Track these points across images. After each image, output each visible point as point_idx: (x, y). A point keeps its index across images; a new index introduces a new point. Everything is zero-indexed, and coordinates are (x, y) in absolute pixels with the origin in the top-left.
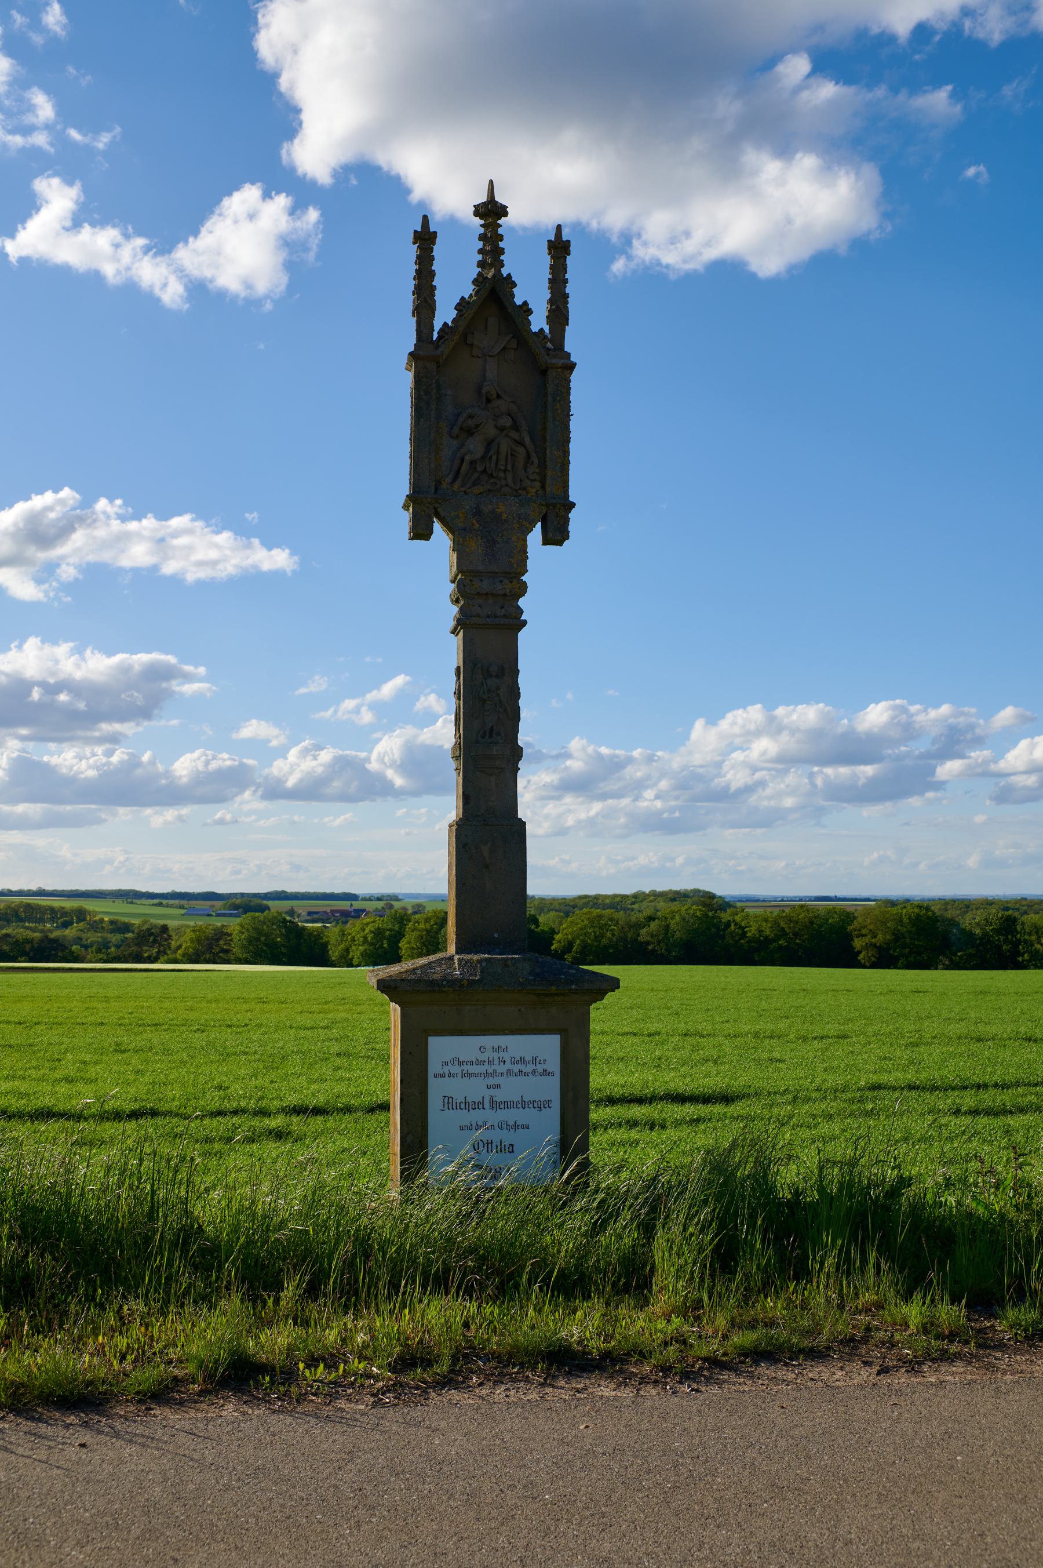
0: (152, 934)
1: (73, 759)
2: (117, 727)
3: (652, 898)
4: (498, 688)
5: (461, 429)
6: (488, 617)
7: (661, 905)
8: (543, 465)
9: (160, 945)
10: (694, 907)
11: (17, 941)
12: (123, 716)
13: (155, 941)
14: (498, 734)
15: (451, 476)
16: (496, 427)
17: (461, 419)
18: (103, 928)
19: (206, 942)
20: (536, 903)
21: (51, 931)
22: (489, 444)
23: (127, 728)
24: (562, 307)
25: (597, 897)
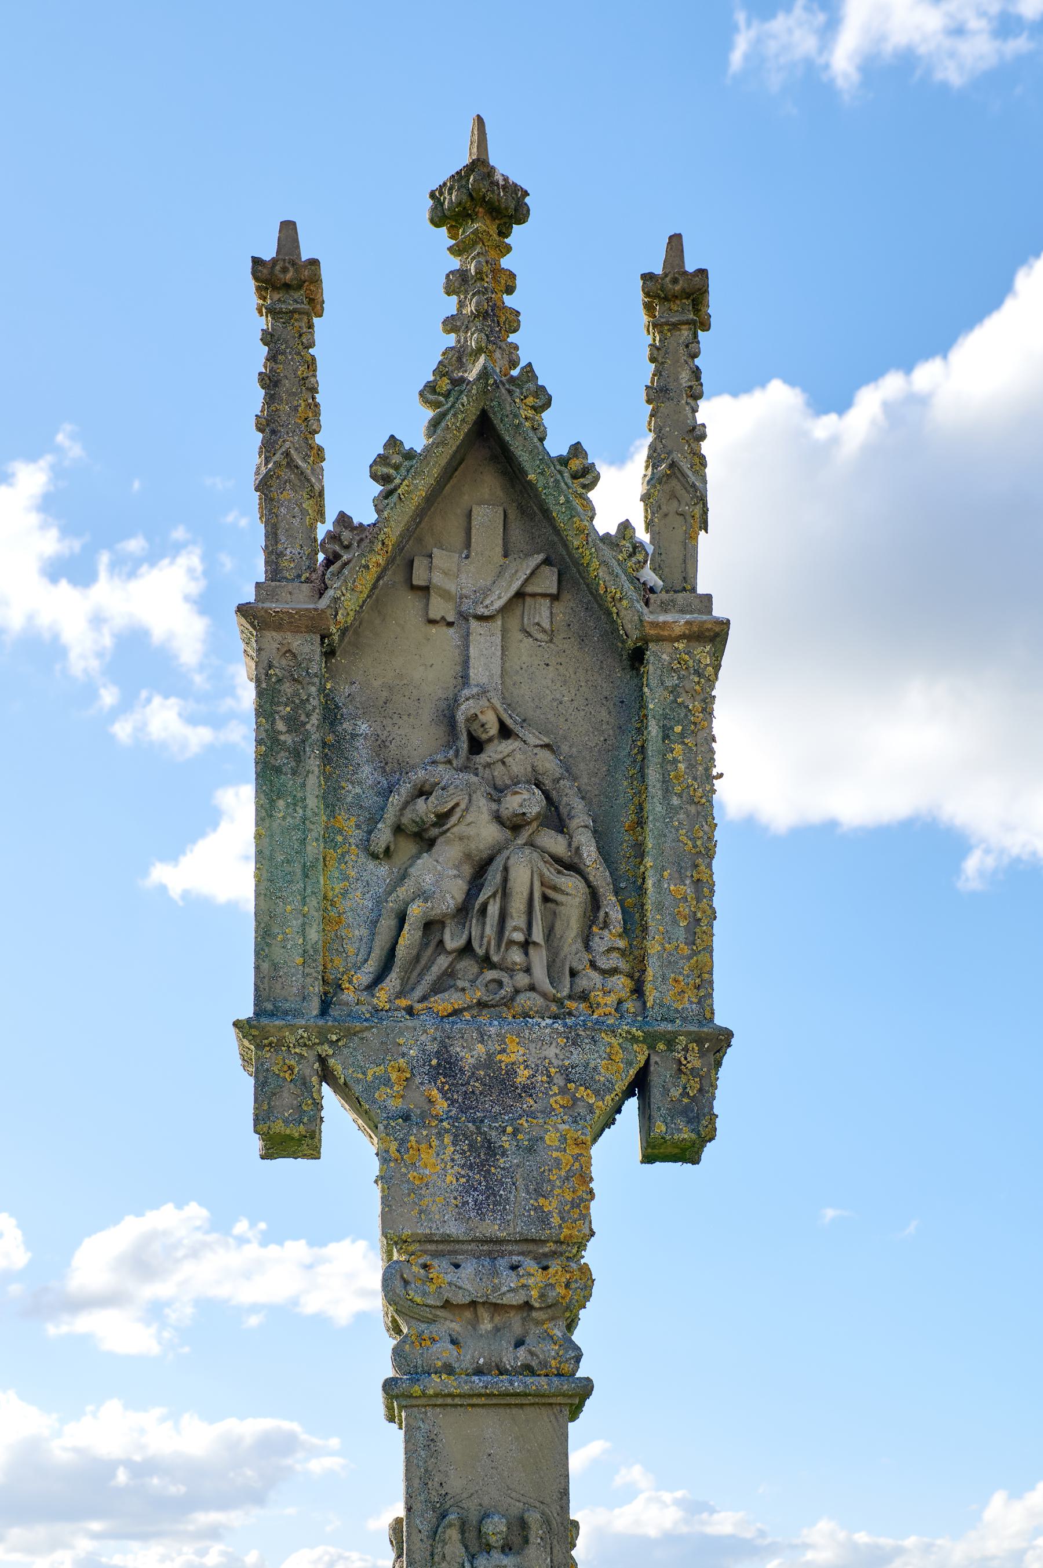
2: (214, 1517)
5: (398, 829)
6: (479, 1372)
12: (224, 1504)
15: (371, 967)
16: (498, 818)
23: (234, 1518)
24: (685, 466)
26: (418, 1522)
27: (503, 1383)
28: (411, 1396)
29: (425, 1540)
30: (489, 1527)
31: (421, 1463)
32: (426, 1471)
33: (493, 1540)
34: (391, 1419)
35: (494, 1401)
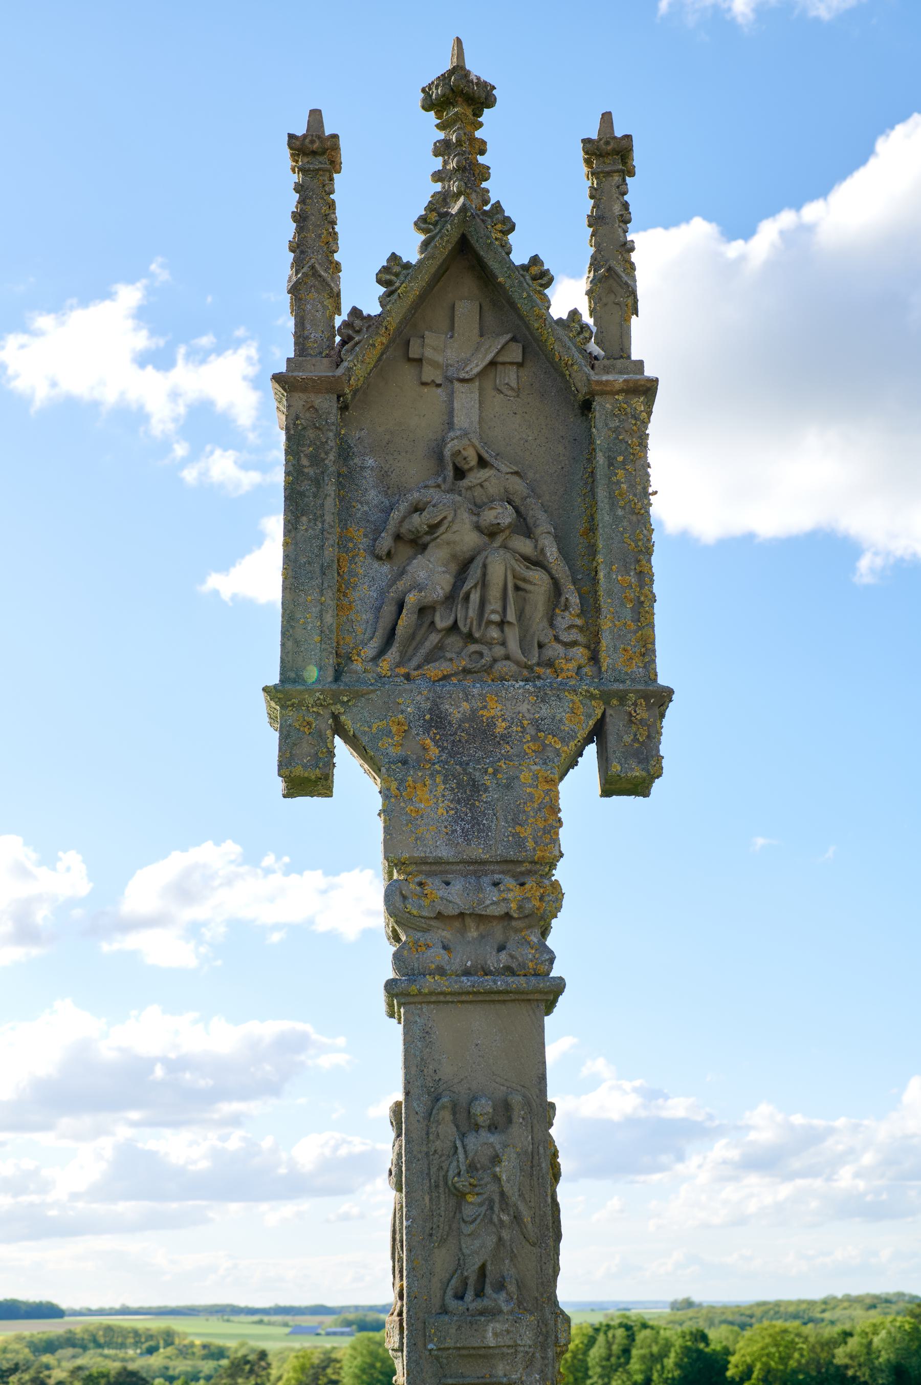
0: (247, 1362)
1: (184, 1148)
2: (236, 1107)
3: (846, 1304)
4: (496, 1159)
5: (398, 537)
6: (467, 973)
7: (859, 1312)
8: (590, 608)
9: (258, 1376)
10: (899, 1319)
11: (90, 1376)
12: (244, 1095)
13: (251, 1371)
14: (500, 1286)
16: (478, 528)
17: (395, 515)
18: (193, 1354)
19: (312, 1372)
20: (704, 1312)
21: (133, 1360)
22: (464, 566)
24: (619, 270)
25: (778, 1304)
26: (415, 1105)
27: (488, 982)
28: (408, 995)
29: (421, 1120)
31: (417, 1053)
32: (422, 1059)
33: (480, 1120)
34: (391, 1015)
35: (480, 998)
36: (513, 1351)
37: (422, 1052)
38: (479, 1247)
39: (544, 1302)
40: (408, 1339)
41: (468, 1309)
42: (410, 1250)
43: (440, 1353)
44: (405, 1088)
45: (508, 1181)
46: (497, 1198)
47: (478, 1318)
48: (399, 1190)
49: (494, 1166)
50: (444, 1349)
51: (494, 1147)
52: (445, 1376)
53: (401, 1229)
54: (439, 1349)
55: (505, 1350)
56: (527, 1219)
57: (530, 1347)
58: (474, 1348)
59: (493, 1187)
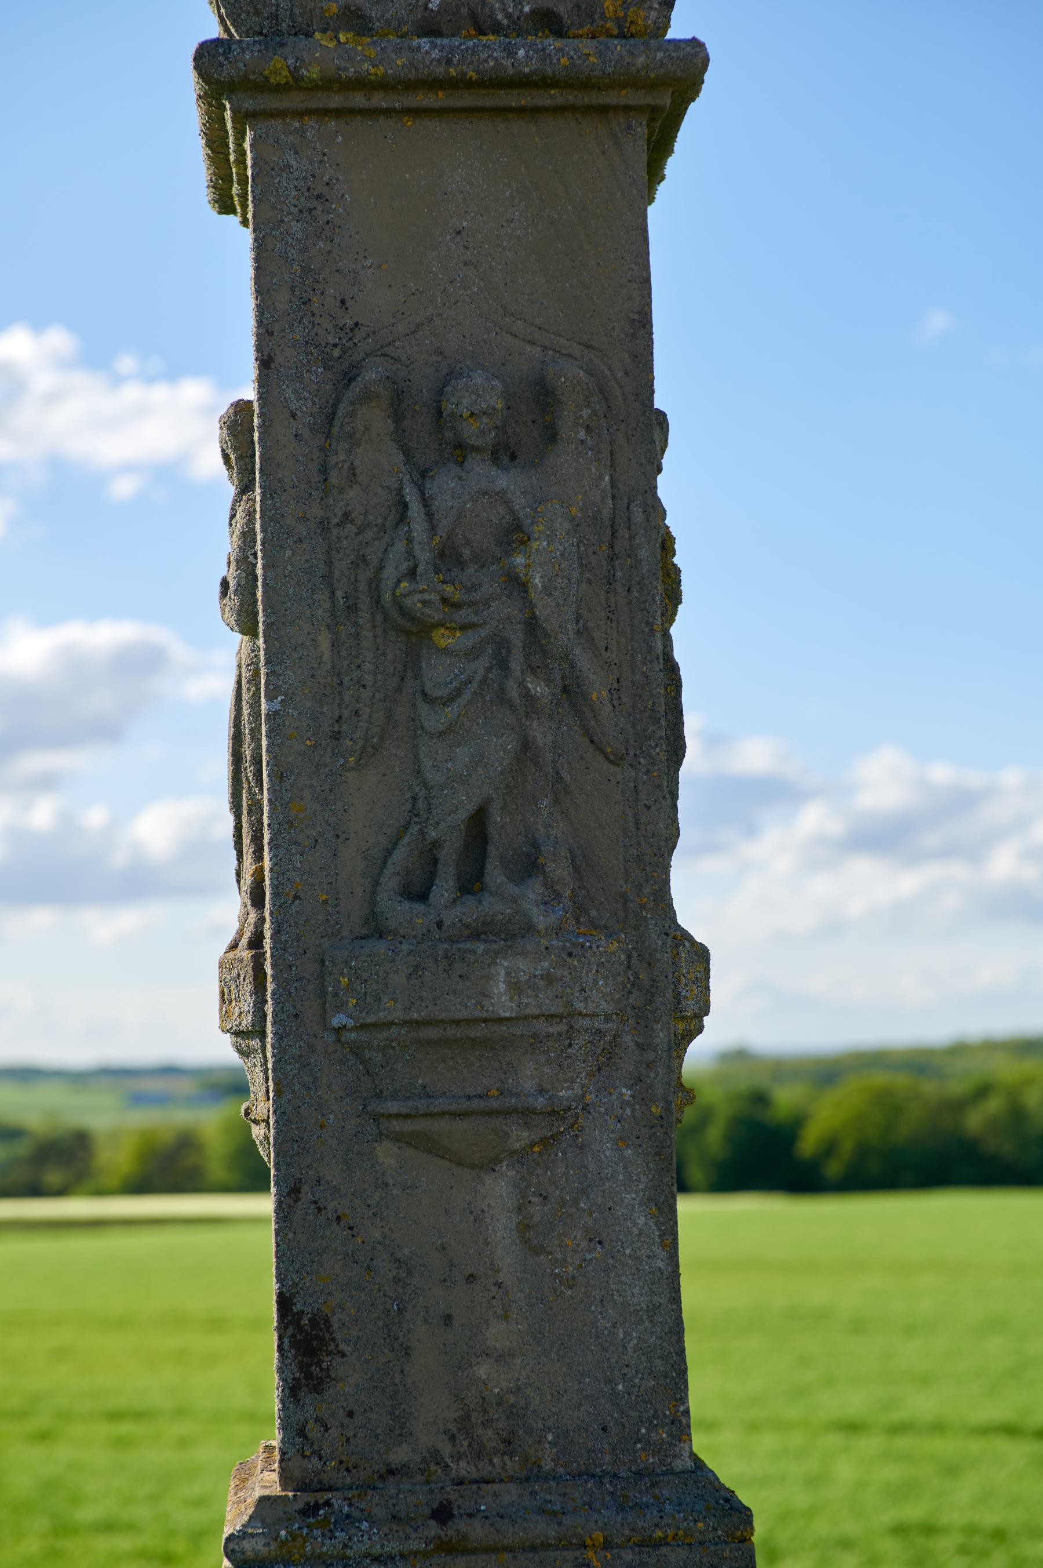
4: (514, 534)
6: (430, 29)
12: (61, 739)
14: (528, 865)
26: (288, 392)
27: (490, 53)
28: (263, 86)
29: (306, 434)
30: (461, 400)
31: (292, 252)
32: (306, 270)
33: (471, 431)
34: (225, 206)
35: (468, 100)
36: (562, 1027)
37: (304, 250)
38: (468, 766)
39: (643, 907)
40: (276, 1003)
41: (440, 925)
42: (278, 777)
43: (364, 1037)
44: (259, 348)
45: (548, 590)
46: (517, 637)
47: (468, 945)
48: (248, 627)
49: (508, 554)
50: (374, 1025)
51: (507, 503)
52: (379, 1095)
53: (255, 731)
54: (363, 1027)
55: (541, 1026)
56: (599, 693)
57: (608, 1018)
58: (457, 1022)
59: (505, 611)
